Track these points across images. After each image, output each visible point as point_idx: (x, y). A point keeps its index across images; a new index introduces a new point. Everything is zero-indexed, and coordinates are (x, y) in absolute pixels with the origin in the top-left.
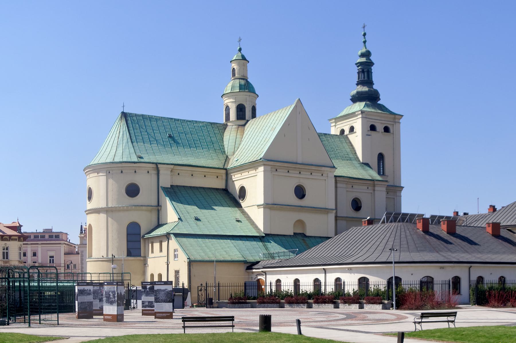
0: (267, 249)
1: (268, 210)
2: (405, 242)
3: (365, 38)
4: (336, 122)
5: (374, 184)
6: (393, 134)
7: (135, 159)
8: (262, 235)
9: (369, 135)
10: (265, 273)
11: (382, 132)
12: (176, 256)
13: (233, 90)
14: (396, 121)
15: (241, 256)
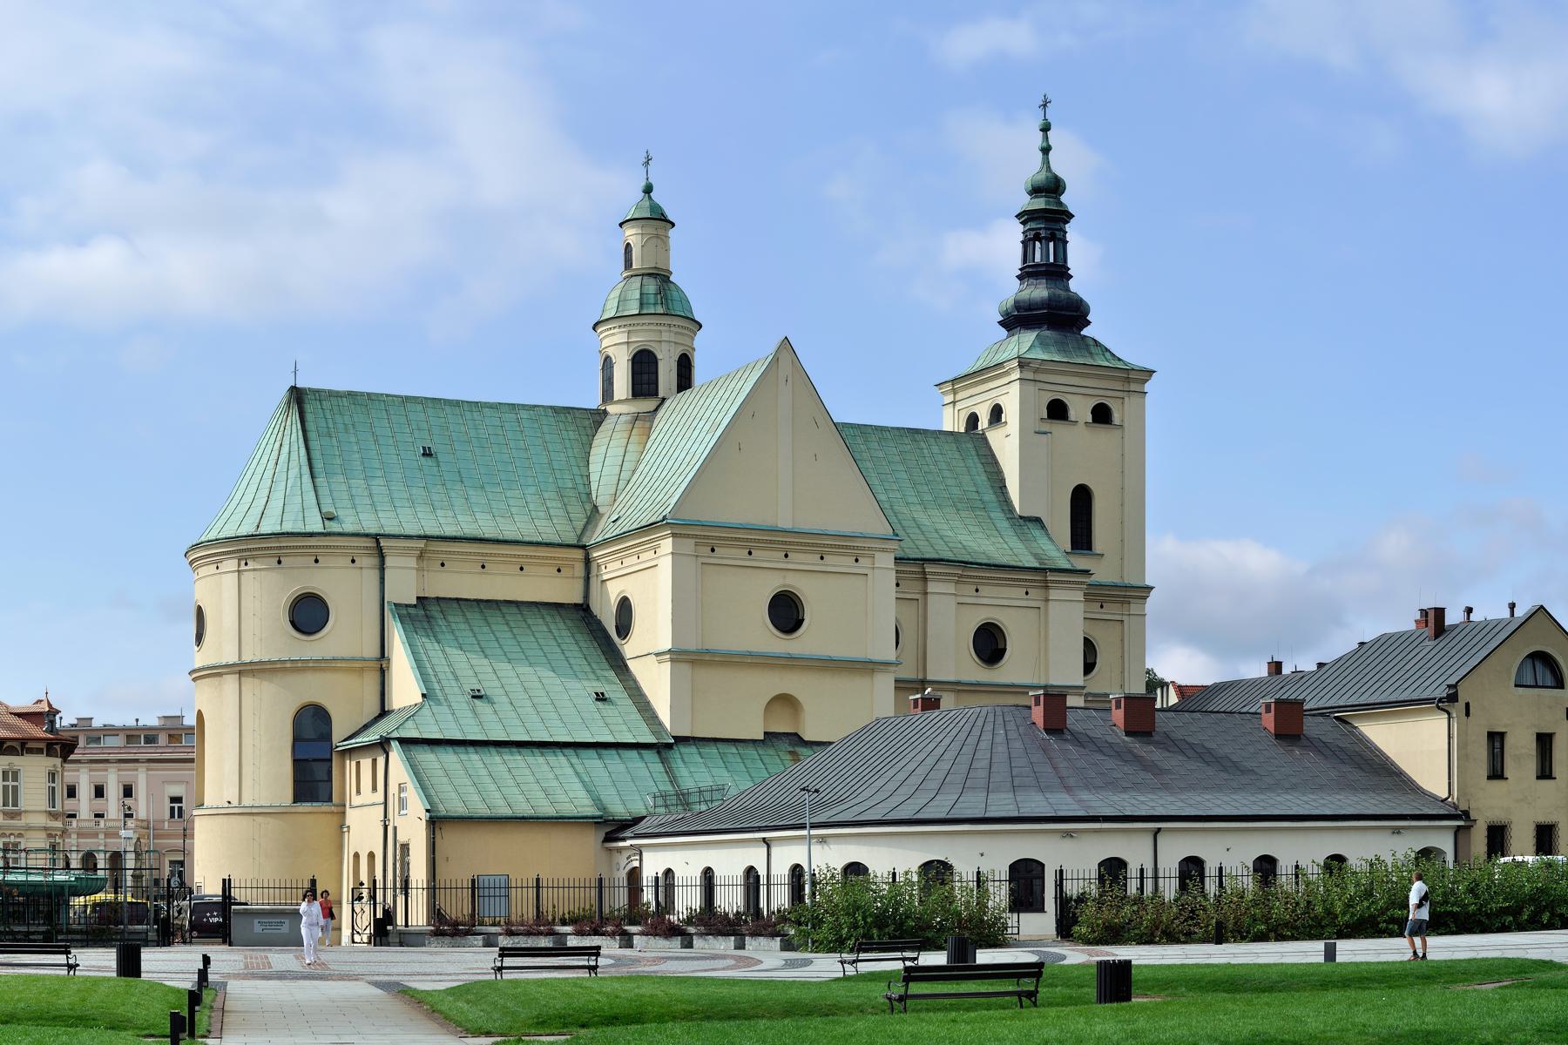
0: (673, 780)
1: (685, 669)
2: (985, 763)
3: (1046, 138)
4: (955, 392)
7: (315, 525)
8: (665, 741)
9: (1046, 433)
12: (402, 804)
13: (623, 310)
15: (588, 802)
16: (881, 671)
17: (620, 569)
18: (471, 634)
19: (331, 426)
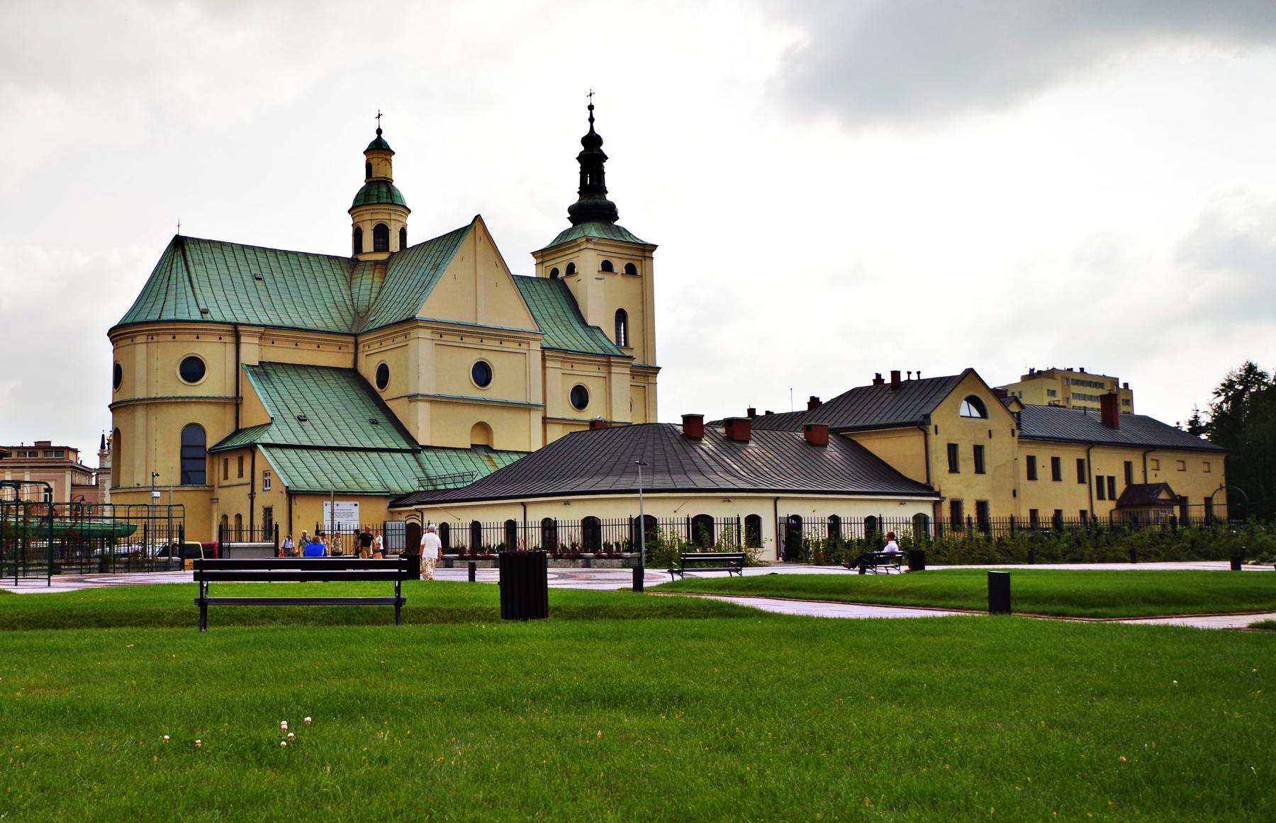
3: (591, 114)
5: (610, 362)
6: (641, 276)
7: (196, 316)
10: (421, 511)
11: (622, 274)
14: (647, 254)
16: (534, 410)
17: (380, 348)
18: (292, 383)
19: (201, 258)
